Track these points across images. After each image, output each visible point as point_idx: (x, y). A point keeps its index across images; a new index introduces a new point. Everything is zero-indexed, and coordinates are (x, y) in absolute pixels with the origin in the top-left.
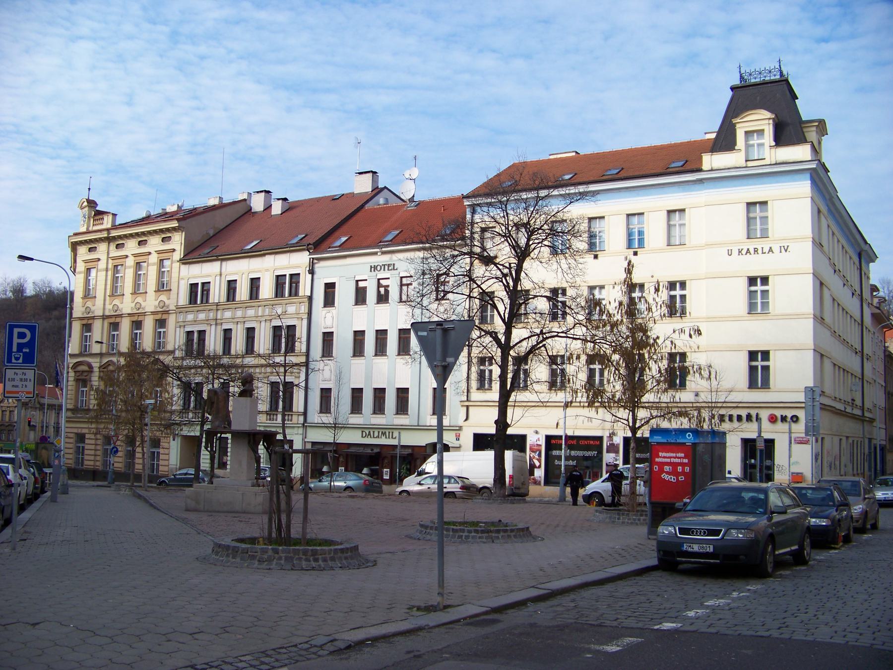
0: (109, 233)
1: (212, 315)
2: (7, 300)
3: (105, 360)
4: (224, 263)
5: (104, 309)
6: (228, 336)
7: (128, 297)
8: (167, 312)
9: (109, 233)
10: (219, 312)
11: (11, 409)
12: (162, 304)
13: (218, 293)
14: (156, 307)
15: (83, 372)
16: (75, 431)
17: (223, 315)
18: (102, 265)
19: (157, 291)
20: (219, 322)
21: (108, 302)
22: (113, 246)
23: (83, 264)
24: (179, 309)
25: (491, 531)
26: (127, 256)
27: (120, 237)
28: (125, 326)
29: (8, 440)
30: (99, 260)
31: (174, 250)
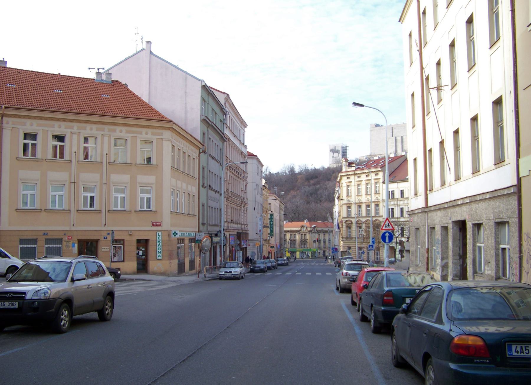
0: (355, 172)
1: (396, 203)
2: (286, 175)
3: (357, 219)
4: (399, 184)
5: (355, 200)
6: (402, 192)
7: (364, 196)
8: (379, 202)
9: (355, 172)
10: (399, 202)
11: (305, 234)
12: (377, 199)
13: (397, 195)
14: (375, 200)
15: (349, 224)
16: (348, 246)
17: (400, 202)
18: (353, 184)
19: (375, 194)
20: (399, 205)
21: (356, 198)
22: (356, 177)
23: (346, 184)
24: (383, 201)
25: (324, 239)
26: (362, 181)
27: (359, 174)
28: (364, 207)
29: (305, 247)
30: (351, 182)
31: (380, 179)
